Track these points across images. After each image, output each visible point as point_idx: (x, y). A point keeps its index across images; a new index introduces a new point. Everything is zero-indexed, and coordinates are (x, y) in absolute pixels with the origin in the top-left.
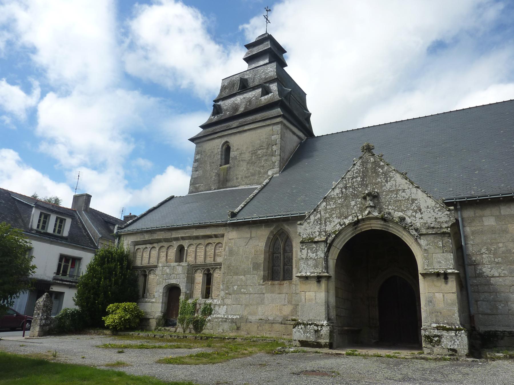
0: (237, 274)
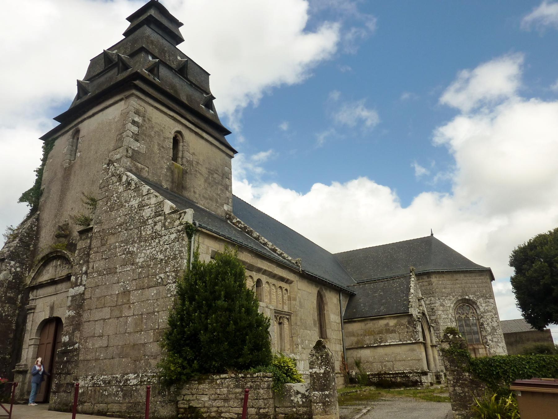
0: (306, 328)
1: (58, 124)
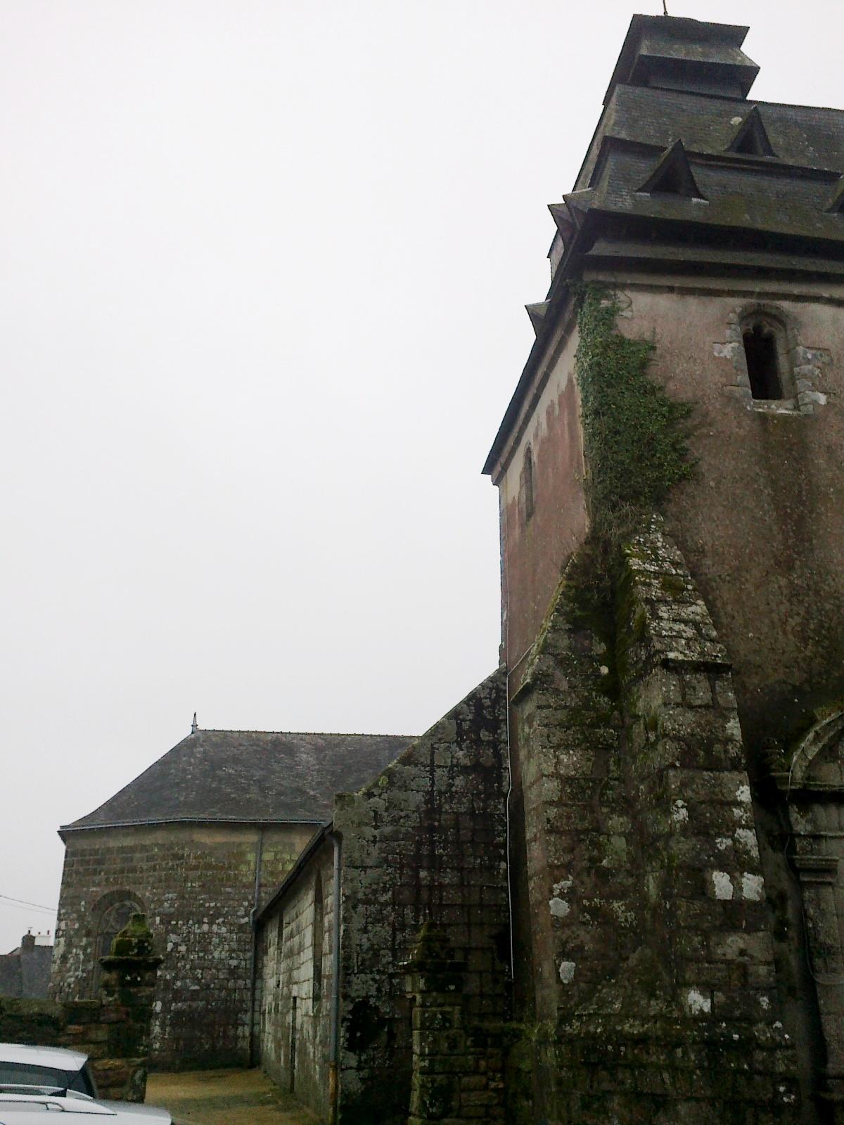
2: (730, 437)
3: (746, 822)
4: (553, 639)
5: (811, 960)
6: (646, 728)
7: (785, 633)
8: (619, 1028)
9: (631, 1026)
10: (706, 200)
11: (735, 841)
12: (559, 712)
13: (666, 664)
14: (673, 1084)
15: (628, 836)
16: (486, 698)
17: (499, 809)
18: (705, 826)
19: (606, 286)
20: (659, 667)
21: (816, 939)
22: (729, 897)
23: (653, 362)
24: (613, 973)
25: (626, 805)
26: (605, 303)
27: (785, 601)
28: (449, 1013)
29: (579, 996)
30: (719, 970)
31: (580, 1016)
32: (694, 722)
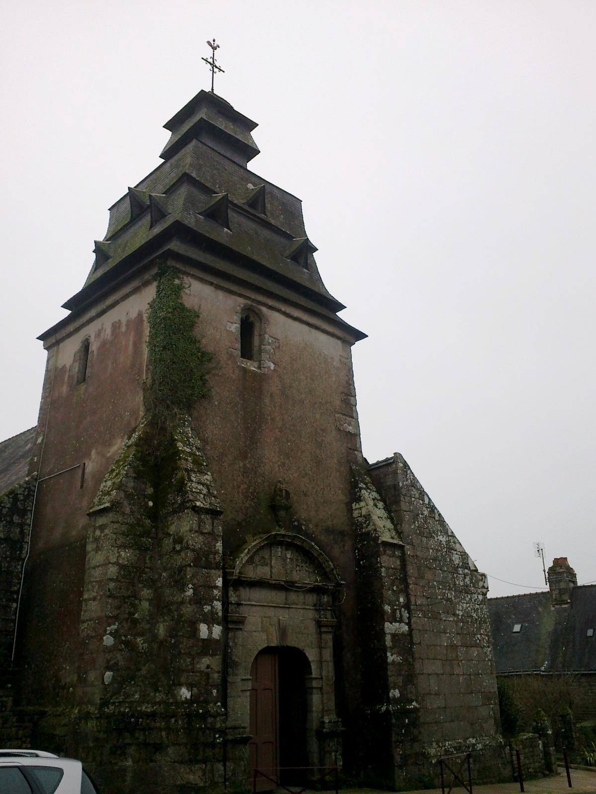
1: (67, 313)
2: (228, 378)
3: (219, 597)
4: (125, 482)
5: (227, 669)
6: (174, 542)
7: (238, 492)
8: (139, 709)
9: (146, 708)
10: (231, 231)
11: (212, 607)
12: (123, 526)
13: (195, 509)
14: (167, 737)
15: (150, 601)
16: (21, 494)
17: (17, 569)
18: (199, 600)
19: (180, 271)
20: (190, 510)
21: (231, 658)
22: (206, 638)
23: (197, 325)
24: (133, 678)
25: (152, 583)
26: (177, 282)
27: (241, 475)
28: (5, 701)
29: (113, 692)
30: (197, 676)
31: (114, 703)
32: (202, 542)
